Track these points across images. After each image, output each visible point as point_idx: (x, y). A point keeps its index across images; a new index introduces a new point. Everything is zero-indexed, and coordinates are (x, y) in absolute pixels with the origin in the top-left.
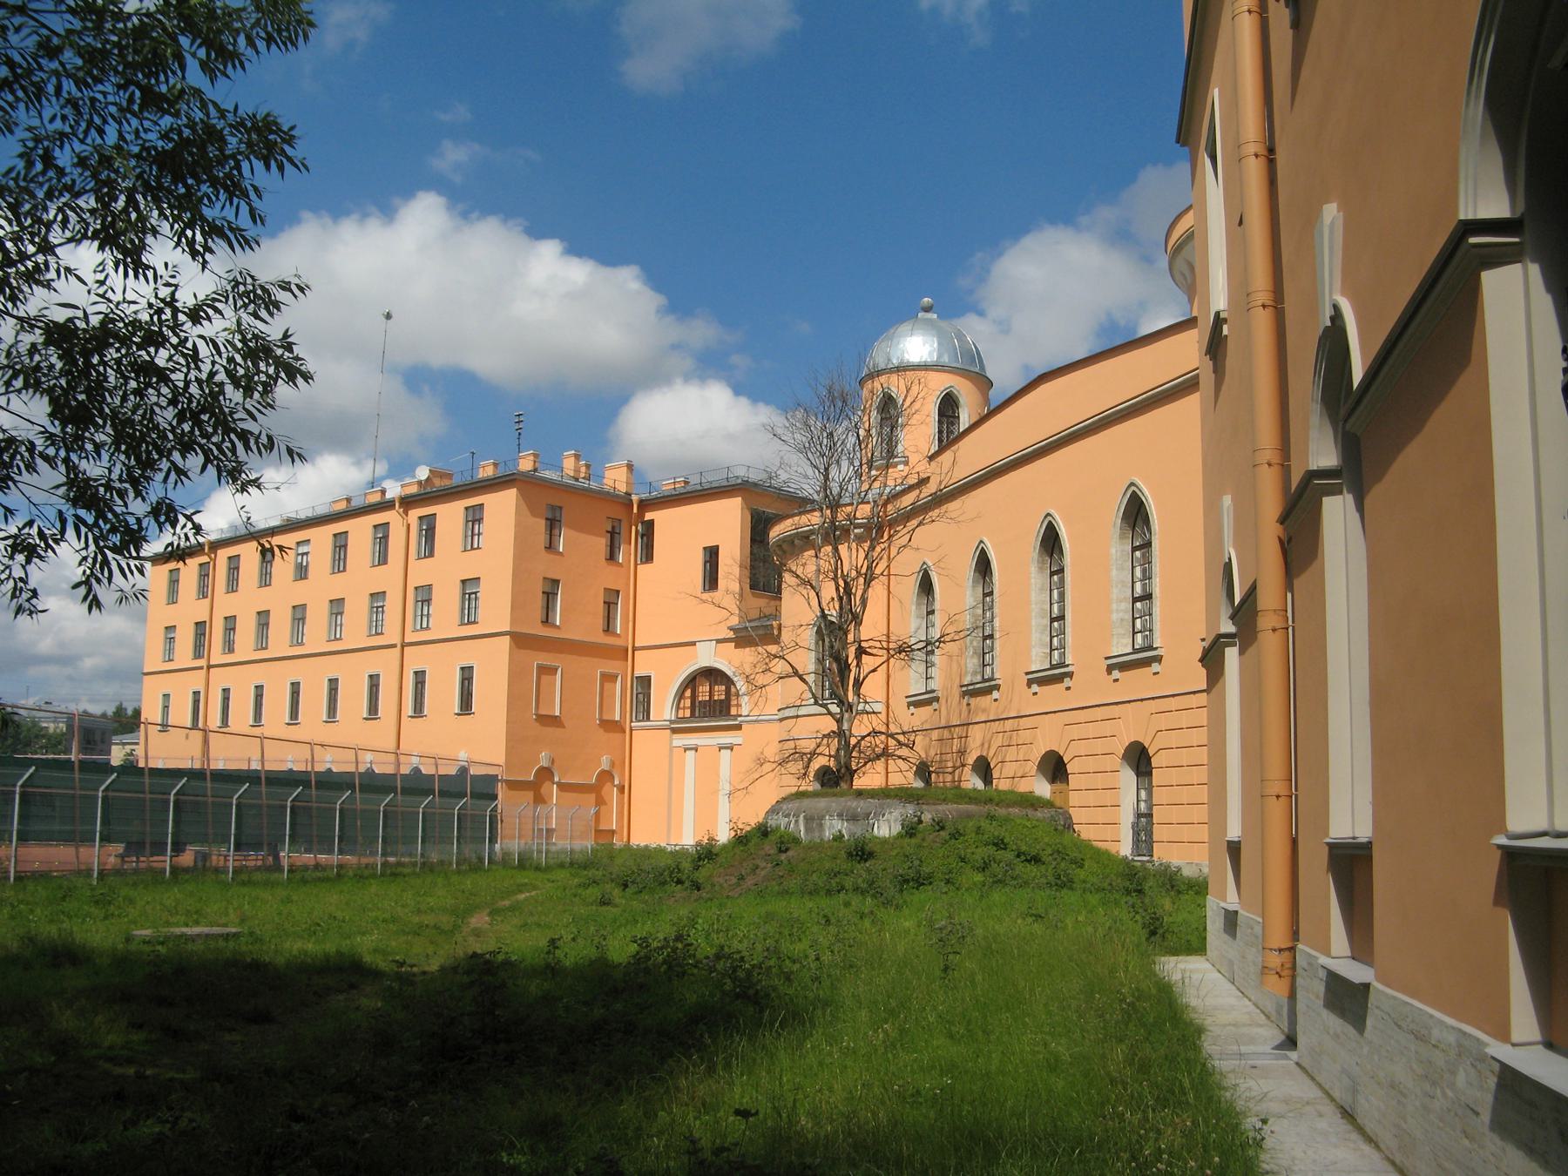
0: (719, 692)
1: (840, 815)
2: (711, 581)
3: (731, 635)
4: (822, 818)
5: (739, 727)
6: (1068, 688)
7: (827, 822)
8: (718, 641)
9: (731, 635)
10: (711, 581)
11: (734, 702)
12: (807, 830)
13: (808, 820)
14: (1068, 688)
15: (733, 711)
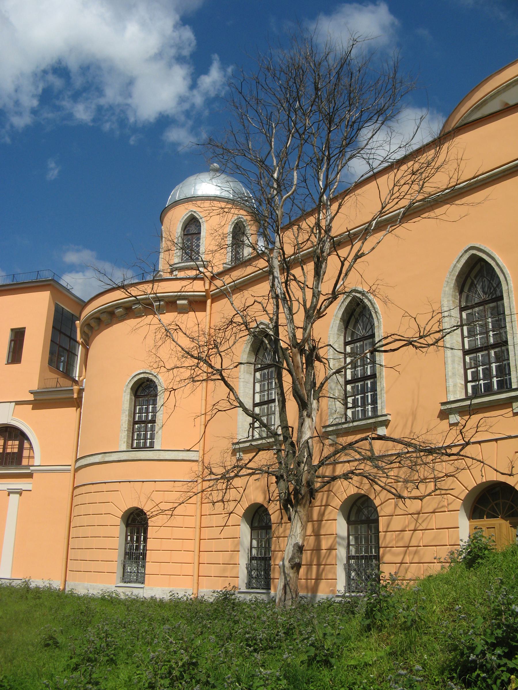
0: (13, 446)
2: (15, 354)
3: (31, 398)
5: (30, 476)
8: (18, 403)
9: (31, 398)
10: (15, 354)
11: (26, 453)
15: (25, 462)
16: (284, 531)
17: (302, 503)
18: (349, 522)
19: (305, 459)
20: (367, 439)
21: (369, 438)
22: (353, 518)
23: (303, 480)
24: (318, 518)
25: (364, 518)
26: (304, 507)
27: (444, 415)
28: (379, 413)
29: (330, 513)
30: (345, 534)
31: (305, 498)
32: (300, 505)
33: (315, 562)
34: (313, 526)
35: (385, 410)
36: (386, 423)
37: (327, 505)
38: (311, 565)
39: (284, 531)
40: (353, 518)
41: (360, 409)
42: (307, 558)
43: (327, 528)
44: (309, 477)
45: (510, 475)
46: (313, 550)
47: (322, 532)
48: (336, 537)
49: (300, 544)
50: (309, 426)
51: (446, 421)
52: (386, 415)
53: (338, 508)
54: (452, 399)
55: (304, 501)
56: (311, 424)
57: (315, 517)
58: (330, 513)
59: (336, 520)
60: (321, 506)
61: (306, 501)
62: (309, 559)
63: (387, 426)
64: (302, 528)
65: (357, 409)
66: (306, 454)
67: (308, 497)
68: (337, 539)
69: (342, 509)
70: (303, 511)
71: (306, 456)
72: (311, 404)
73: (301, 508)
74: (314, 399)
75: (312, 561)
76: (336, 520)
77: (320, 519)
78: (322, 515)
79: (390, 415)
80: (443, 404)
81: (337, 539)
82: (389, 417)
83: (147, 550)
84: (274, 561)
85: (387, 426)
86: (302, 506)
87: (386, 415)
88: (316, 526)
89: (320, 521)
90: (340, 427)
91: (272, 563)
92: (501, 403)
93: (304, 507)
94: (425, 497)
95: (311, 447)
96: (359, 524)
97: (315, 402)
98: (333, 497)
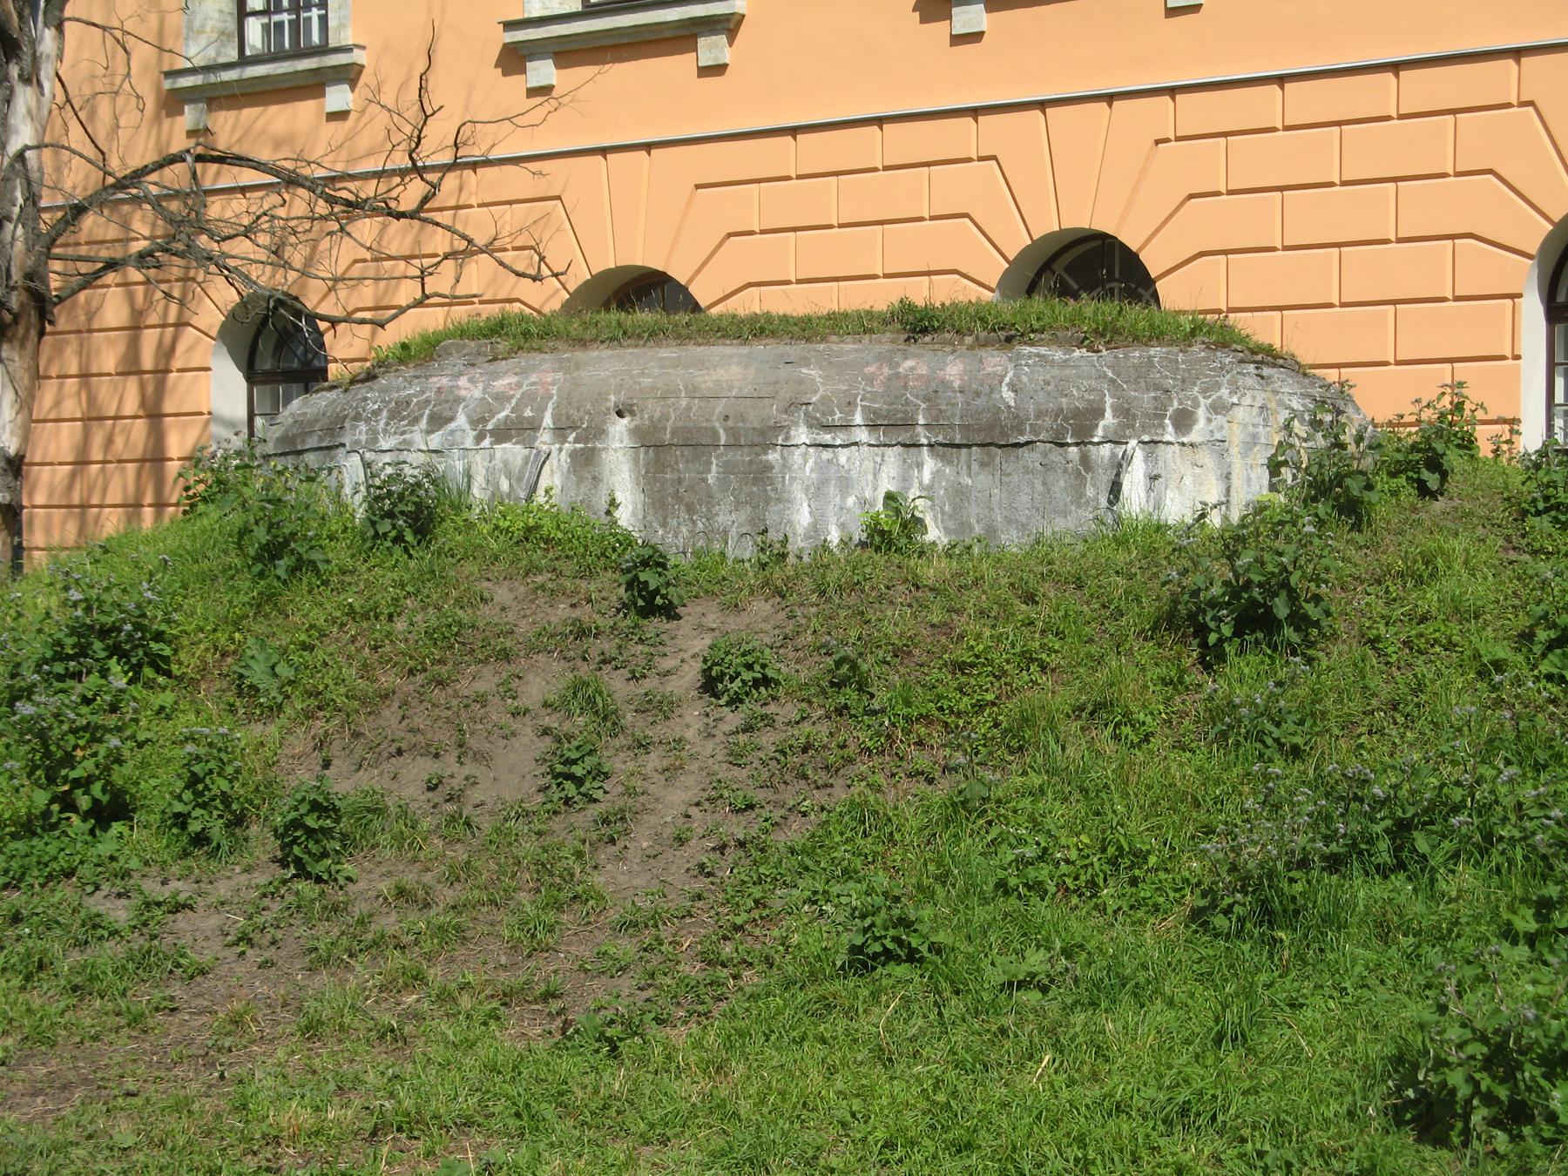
1: (893, 427)
4: (768, 436)
6: (718, 70)
7: (800, 459)
12: (662, 492)
13: (656, 448)
14: (718, 70)
16: (58, 403)
17: (14, 335)
18: (252, 376)
19: (17, 210)
20: (184, 160)
21: (189, 158)
22: (265, 364)
23: (14, 270)
24: (157, 362)
25: (295, 364)
26: (23, 346)
27: (513, 59)
28: (333, 43)
29: (189, 350)
30: (242, 413)
31: (23, 323)
32: (10, 341)
33: (149, 498)
34: (142, 387)
35: (349, 32)
36: (349, 75)
37: (181, 324)
38: (138, 505)
39: (58, 403)
40: (265, 364)
41: (285, 17)
42: (125, 486)
43: (182, 393)
44: (29, 263)
45: (534, 279)
46: (142, 461)
47: (168, 407)
48: (207, 423)
49: (12, 451)
50: (29, 112)
51: (516, 79)
52: (347, 49)
53: (214, 333)
54: (536, 14)
55: (21, 331)
56: (33, 104)
57: (147, 362)
58: (189, 350)
59: (208, 369)
60: (164, 326)
61: (27, 331)
62: (131, 488)
63: (353, 83)
64: (17, 406)
65: (276, 18)
66: (18, 194)
67: (34, 319)
68: (213, 428)
69: (227, 335)
70: (21, 357)
71: (20, 201)
72: (34, 43)
73: (12, 349)
74: (46, 25)
75: (140, 493)
76: (208, 369)
77: (161, 367)
78: (167, 353)
79: (363, 48)
80: (509, 26)
81: (213, 428)
82: (358, 57)
83: (1153, 282)
84: (30, 496)
85: (353, 83)
86: (16, 343)
87: (347, 49)
88: (150, 389)
89: (162, 372)
90: (212, 79)
91: (25, 503)
92: (667, 34)
93: (23, 346)
94: (340, 321)
95: (35, 176)
96: (280, 382)
97: (49, 35)
98: (200, 301)
